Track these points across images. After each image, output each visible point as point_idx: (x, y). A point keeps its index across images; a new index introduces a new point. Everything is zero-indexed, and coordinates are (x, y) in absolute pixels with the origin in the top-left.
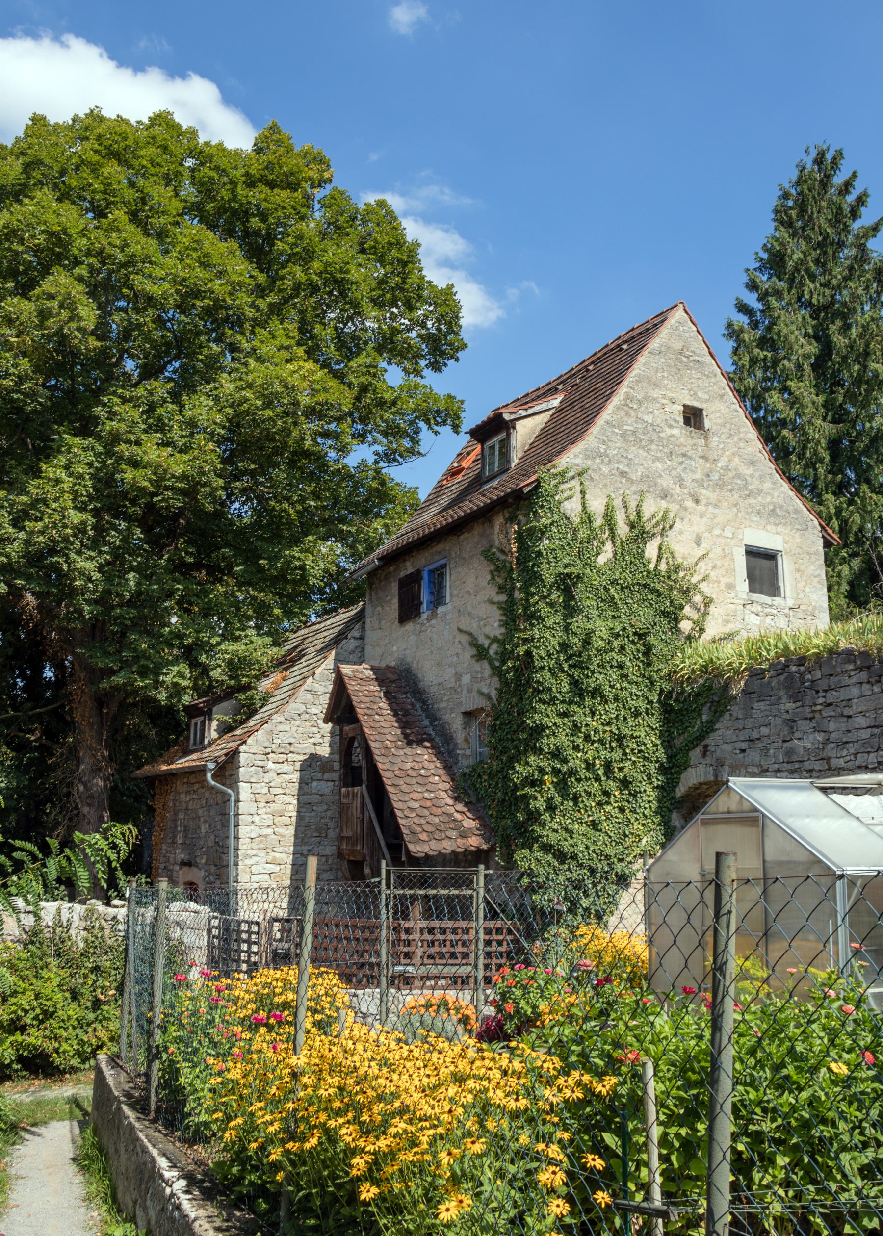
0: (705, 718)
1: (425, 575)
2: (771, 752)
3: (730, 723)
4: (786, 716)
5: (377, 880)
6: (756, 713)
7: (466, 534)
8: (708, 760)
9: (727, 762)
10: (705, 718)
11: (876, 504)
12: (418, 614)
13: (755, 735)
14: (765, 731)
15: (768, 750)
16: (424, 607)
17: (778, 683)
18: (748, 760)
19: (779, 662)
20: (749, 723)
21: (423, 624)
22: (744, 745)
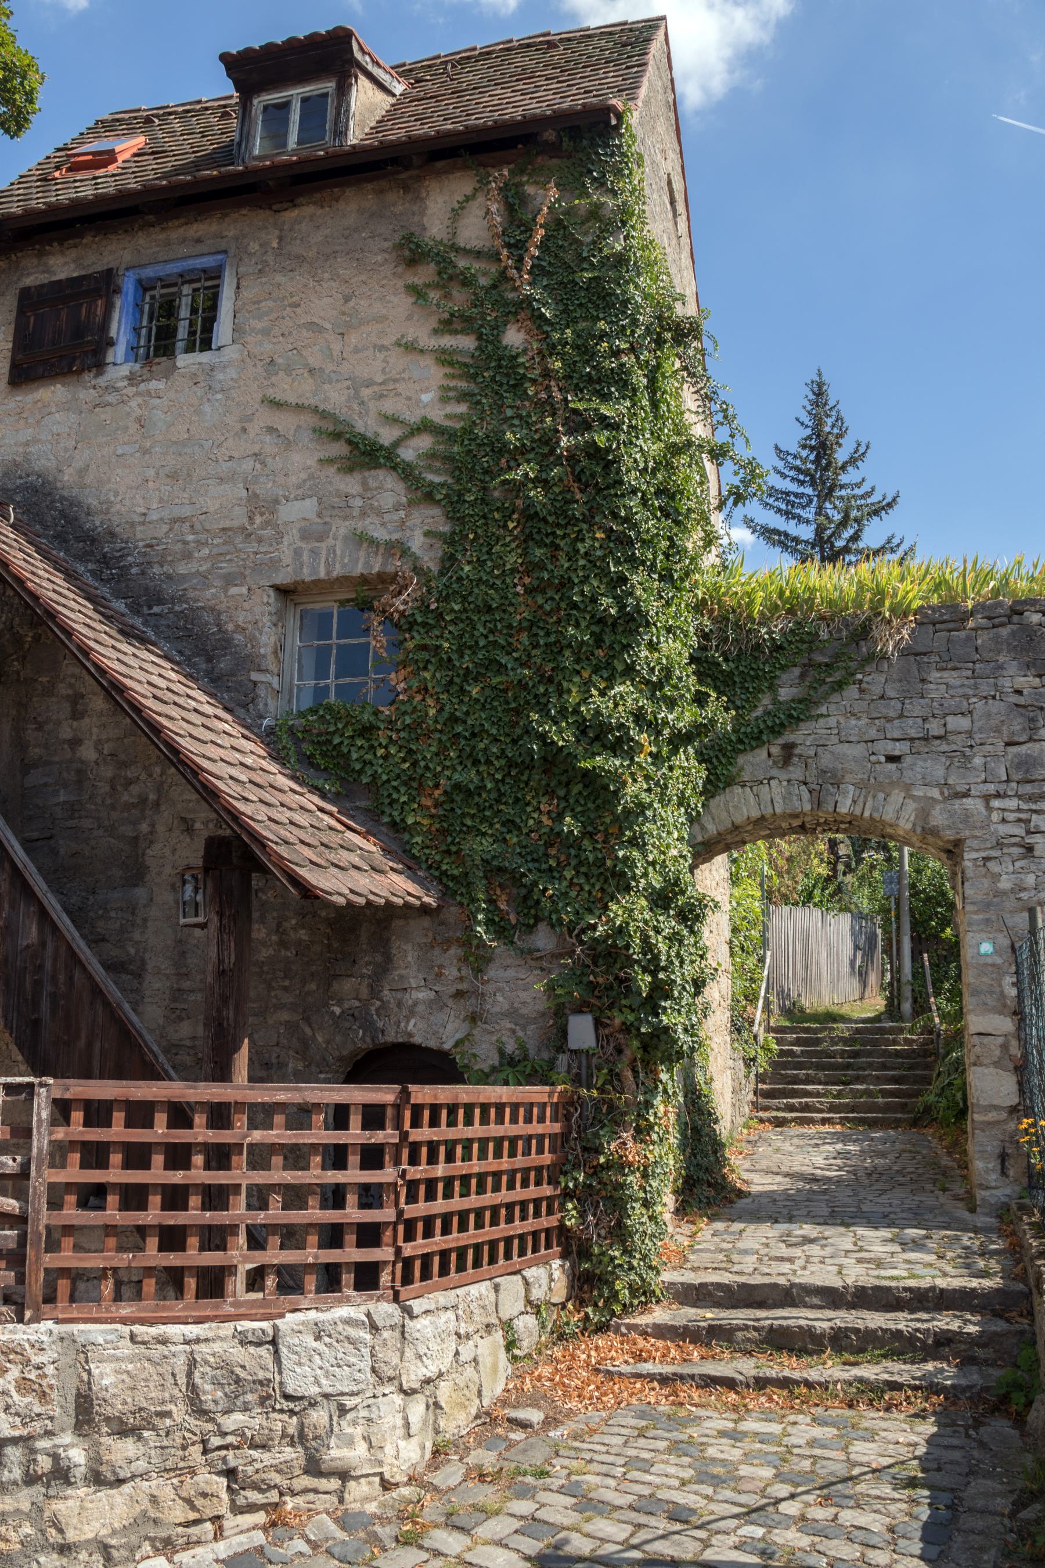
0: (785, 693)
1: (128, 284)
2: (978, 761)
3: (860, 706)
4: (1015, 699)
5: (342, 681)
6: (935, 691)
7: (310, 210)
8: (796, 772)
9: (848, 778)
10: (785, 693)
11: (600, 1008)
12: (99, 366)
13: (935, 727)
14: (956, 723)
15: (969, 759)
16: (118, 353)
17: (996, 640)
18: (908, 776)
19: (1000, 604)
20: (916, 708)
21: (111, 388)
22: (898, 748)
